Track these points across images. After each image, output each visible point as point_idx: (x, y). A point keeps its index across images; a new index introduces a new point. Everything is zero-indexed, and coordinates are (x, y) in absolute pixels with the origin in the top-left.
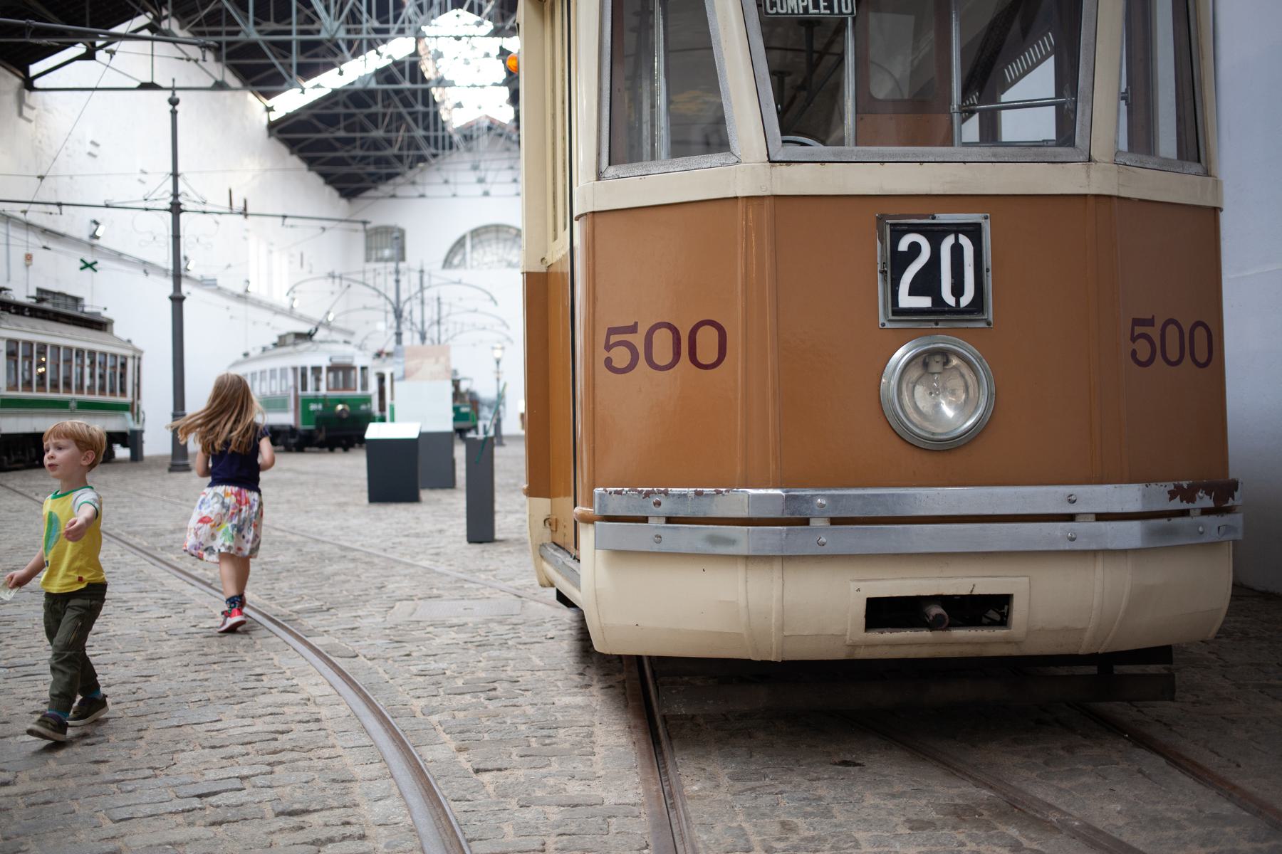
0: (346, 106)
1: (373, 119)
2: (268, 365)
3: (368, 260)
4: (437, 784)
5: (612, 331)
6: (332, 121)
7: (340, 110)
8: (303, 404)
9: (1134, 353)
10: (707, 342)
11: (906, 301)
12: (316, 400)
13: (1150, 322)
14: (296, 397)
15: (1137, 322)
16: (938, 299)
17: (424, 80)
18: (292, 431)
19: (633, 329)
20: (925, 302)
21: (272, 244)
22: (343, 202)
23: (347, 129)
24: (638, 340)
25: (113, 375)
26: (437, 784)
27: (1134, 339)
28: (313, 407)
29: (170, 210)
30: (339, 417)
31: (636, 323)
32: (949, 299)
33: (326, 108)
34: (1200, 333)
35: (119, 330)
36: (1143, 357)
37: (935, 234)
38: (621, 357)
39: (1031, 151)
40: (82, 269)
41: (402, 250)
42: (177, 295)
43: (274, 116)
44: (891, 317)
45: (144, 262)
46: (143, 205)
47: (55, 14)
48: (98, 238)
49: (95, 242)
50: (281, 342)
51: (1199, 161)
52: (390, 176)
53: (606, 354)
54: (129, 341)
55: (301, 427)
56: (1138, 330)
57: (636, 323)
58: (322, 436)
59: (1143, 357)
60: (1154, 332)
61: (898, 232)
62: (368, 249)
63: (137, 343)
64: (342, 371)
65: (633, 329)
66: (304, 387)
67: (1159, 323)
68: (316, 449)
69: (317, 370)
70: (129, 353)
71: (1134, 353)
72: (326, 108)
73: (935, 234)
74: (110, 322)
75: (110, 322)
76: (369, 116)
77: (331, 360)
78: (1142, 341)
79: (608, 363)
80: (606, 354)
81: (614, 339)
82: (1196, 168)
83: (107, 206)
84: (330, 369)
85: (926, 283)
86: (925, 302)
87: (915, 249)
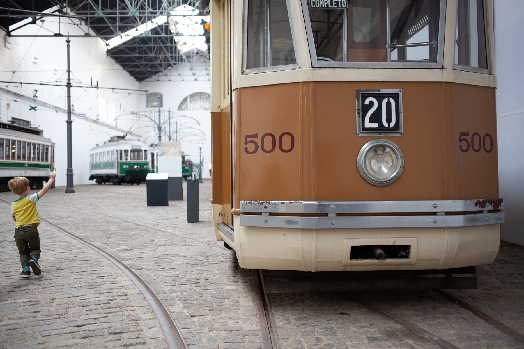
0: (139, 44)
1: (150, 49)
2: (106, 149)
3: (147, 107)
6: (133, 50)
7: (136, 45)
8: (121, 165)
9: (461, 147)
12: (126, 164)
13: (467, 134)
14: (118, 163)
15: (462, 134)
16: (381, 124)
17: (171, 33)
18: (116, 176)
19: (256, 136)
20: (375, 125)
21: (108, 100)
22: (138, 83)
23: (139, 53)
24: (258, 140)
25: (43, 153)
28: (125, 166)
29: (66, 86)
30: (135, 171)
31: (257, 134)
32: (385, 124)
33: (131, 44)
34: (488, 139)
35: (45, 135)
36: (464, 147)
37: (380, 98)
38: (251, 147)
40: (30, 109)
41: (161, 102)
42: (69, 120)
43: (109, 48)
44: (361, 131)
45: (56, 107)
46: (56, 83)
48: (37, 97)
49: (36, 98)
50: (112, 140)
51: (487, 68)
52: (157, 72)
53: (245, 146)
54: (49, 139)
55: (120, 175)
57: (257, 134)
58: (128, 179)
59: (464, 147)
60: (469, 138)
62: (148, 102)
63: (53, 140)
64: (137, 152)
65: (256, 136)
66: (121, 159)
68: (98, 175)
69: (126, 151)
70: (49, 144)
71: (461, 147)
72: (131, 44)
73: (380, 98)
74: (42, 131)
75: (42, 131)
76: (148, 48)
77: (132, 147)
78: (464, 142)
79: (246, 149)
81: (248, 140)
82: (486, 71)
83: (41, 84)
84: (131, 151)
86: (375, 125)
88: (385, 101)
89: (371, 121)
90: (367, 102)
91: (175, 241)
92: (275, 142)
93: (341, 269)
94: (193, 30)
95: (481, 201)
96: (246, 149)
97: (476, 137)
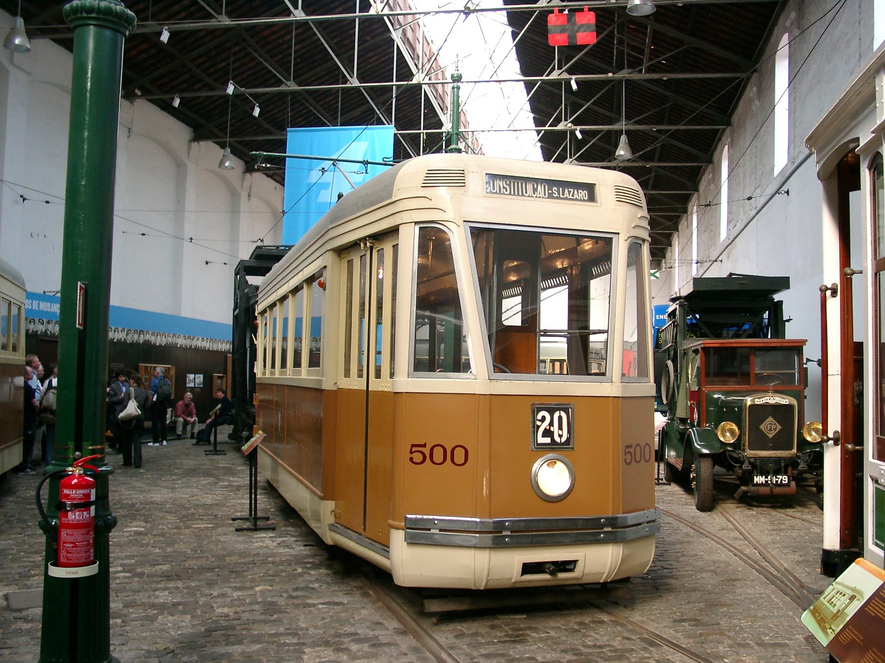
4: (767, 550)
5: (413, 446)
9: (625, 459)
10: (459, 455)
11: (541, 440)
13: (630, 447)
15: (627, 447)
16: (553, 440)
19: (424, 446)
20: (548, 440)
24: (427, 451)
26: (767, 550)
27: (625, 454)
31: (426, 444)
32: (557, 439)
34: (647, 448)
36: (628, 461)
37: (551, 412)
38: (418, 457)
39: (655, 317)
44: (536, 446)
47: (331, 124)
53: (411, 456)
56: (628, 450)
57: (426, 444)
59: (628, 461)
60: (632, 450)
61: (539, 410)
65: (424, 446)
67: (634, 447)
73: (551, 412)
78: (629, 455)
79: (411, 459)
80: (411, 456)
81: (414, 449)
83: (446, 40)
85: (548, 433)
86: (548, 440)
87: (543, 419)
88: (557, 415)
89: (543, 436)
90: (539, 417)
91: (177, 588)
92: (871, 573)
93: (509, 586)
94: (191, 239)
95: (109, 431)
96: (411, 459)
97: (638, 460)
